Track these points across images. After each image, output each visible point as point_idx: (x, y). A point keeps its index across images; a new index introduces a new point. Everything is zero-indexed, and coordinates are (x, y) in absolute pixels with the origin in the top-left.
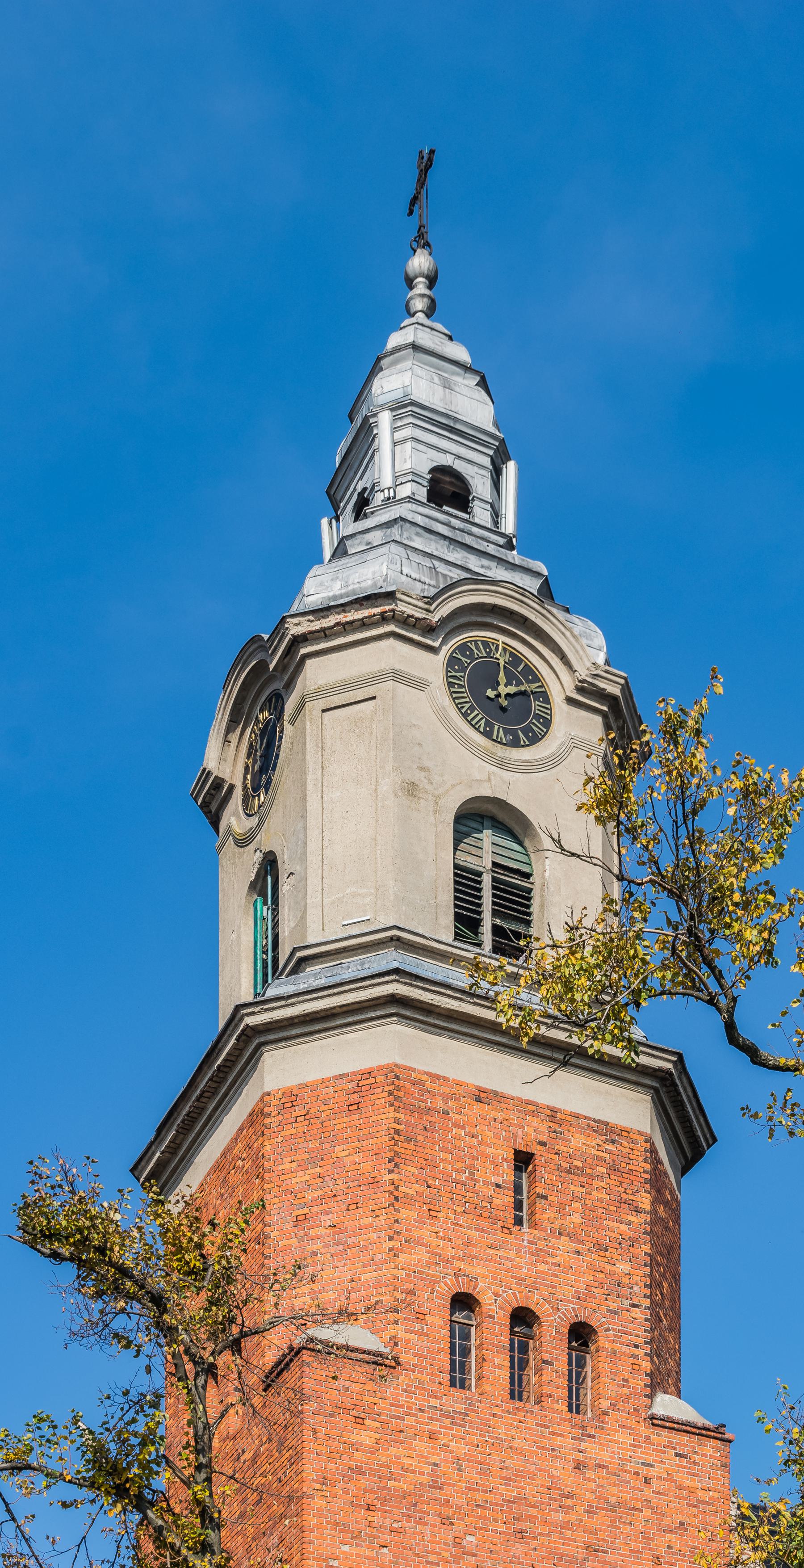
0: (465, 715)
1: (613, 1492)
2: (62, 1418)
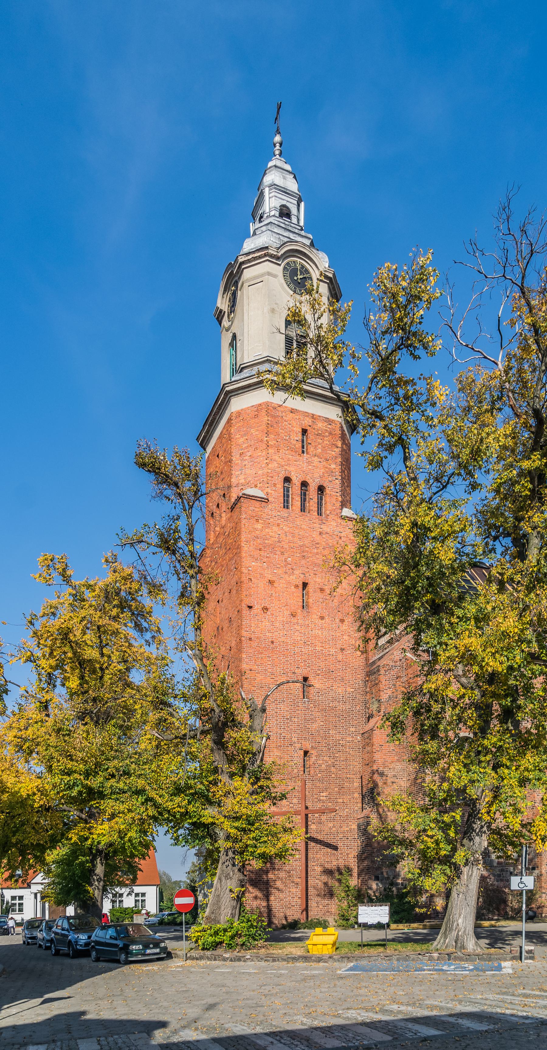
0: (288, 286)
2: (152, 525)
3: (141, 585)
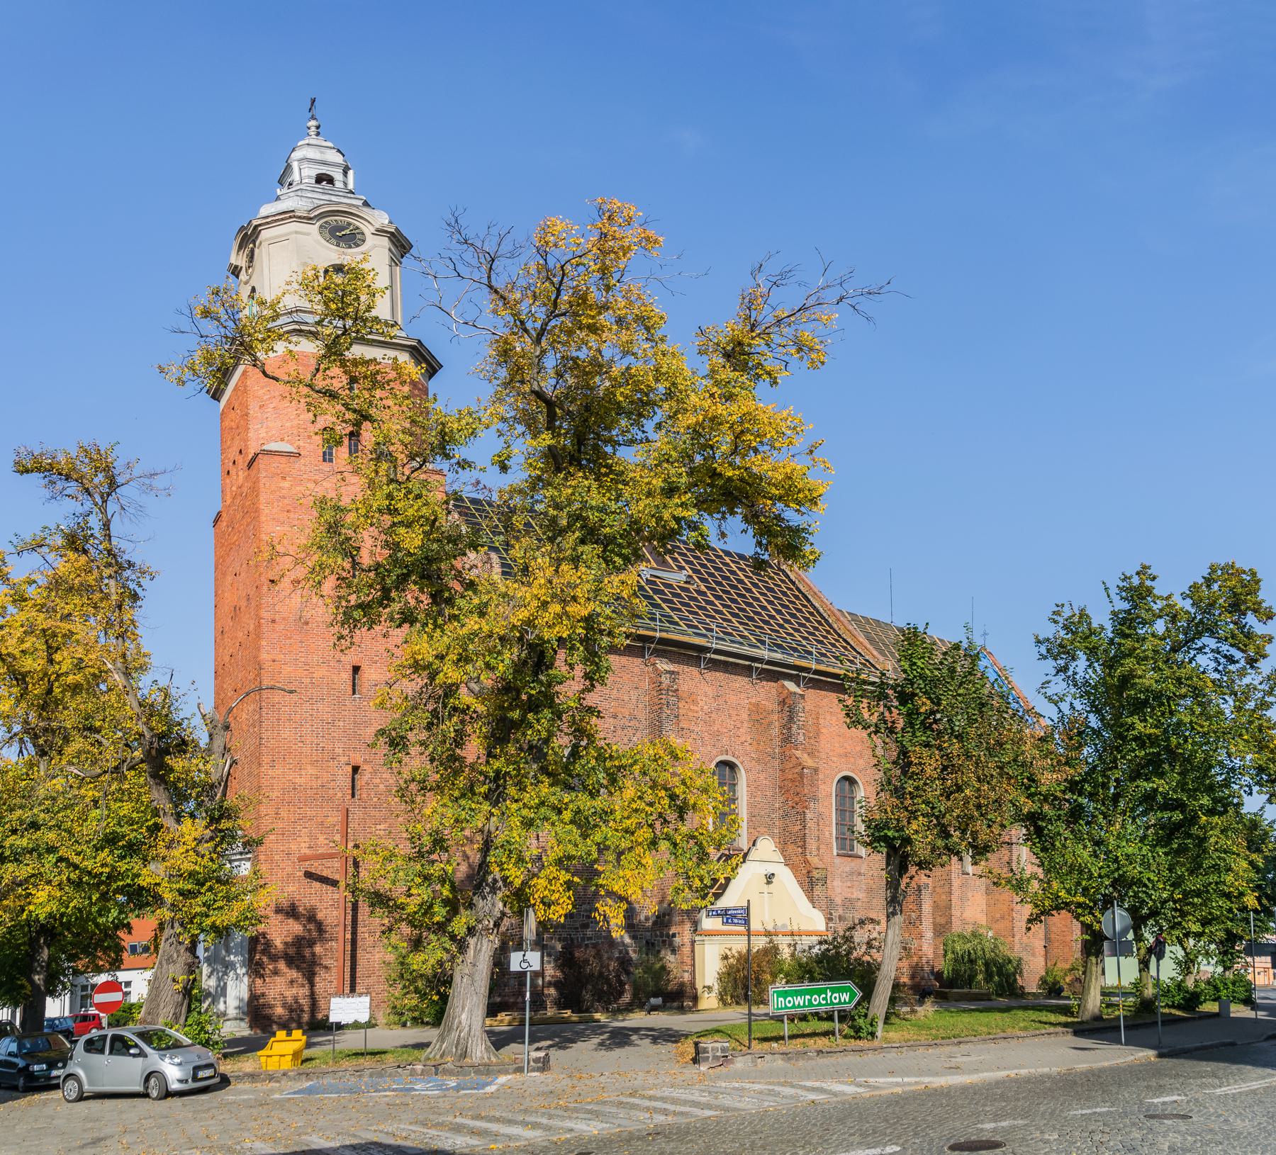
2: (53, 527)
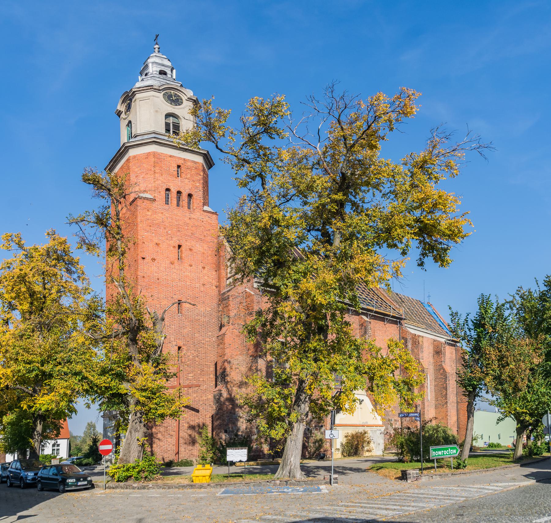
1: (196, 224)
2: (91, 211)
3: (82, 245)
